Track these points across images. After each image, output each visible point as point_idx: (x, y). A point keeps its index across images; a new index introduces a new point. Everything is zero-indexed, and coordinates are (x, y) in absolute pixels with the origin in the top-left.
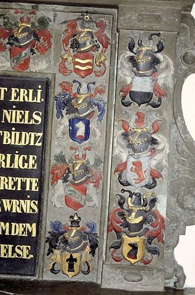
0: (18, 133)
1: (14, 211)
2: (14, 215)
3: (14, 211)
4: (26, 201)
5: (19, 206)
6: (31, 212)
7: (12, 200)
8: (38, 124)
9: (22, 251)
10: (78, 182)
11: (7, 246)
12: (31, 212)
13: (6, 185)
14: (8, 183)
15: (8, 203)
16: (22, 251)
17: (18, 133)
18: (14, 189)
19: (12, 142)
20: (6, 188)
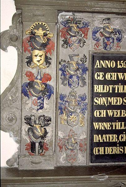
0: (122, 86)
1: (100, 129)
2: (95, 143)
3: (100, 129)
4: (107, 123)
5: (103, 126)
6: (120, 153)
7: (113, 110)
8: (96, 98)
9: (119, 150)
10: (71, 34)
11: (117, 111)
12: (120, 153)
13: (116, 151)
14: (117, 150)
15: (111, 112)
16: (119, 150)
17: (122, 86)
18: (106, 135)
19: (99, 91)
20: (116, 153)
